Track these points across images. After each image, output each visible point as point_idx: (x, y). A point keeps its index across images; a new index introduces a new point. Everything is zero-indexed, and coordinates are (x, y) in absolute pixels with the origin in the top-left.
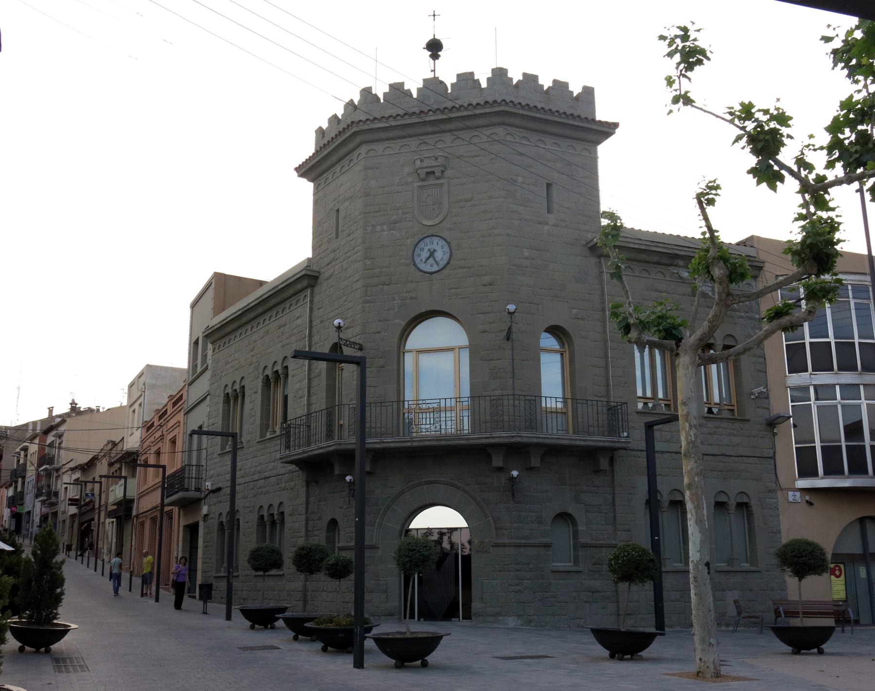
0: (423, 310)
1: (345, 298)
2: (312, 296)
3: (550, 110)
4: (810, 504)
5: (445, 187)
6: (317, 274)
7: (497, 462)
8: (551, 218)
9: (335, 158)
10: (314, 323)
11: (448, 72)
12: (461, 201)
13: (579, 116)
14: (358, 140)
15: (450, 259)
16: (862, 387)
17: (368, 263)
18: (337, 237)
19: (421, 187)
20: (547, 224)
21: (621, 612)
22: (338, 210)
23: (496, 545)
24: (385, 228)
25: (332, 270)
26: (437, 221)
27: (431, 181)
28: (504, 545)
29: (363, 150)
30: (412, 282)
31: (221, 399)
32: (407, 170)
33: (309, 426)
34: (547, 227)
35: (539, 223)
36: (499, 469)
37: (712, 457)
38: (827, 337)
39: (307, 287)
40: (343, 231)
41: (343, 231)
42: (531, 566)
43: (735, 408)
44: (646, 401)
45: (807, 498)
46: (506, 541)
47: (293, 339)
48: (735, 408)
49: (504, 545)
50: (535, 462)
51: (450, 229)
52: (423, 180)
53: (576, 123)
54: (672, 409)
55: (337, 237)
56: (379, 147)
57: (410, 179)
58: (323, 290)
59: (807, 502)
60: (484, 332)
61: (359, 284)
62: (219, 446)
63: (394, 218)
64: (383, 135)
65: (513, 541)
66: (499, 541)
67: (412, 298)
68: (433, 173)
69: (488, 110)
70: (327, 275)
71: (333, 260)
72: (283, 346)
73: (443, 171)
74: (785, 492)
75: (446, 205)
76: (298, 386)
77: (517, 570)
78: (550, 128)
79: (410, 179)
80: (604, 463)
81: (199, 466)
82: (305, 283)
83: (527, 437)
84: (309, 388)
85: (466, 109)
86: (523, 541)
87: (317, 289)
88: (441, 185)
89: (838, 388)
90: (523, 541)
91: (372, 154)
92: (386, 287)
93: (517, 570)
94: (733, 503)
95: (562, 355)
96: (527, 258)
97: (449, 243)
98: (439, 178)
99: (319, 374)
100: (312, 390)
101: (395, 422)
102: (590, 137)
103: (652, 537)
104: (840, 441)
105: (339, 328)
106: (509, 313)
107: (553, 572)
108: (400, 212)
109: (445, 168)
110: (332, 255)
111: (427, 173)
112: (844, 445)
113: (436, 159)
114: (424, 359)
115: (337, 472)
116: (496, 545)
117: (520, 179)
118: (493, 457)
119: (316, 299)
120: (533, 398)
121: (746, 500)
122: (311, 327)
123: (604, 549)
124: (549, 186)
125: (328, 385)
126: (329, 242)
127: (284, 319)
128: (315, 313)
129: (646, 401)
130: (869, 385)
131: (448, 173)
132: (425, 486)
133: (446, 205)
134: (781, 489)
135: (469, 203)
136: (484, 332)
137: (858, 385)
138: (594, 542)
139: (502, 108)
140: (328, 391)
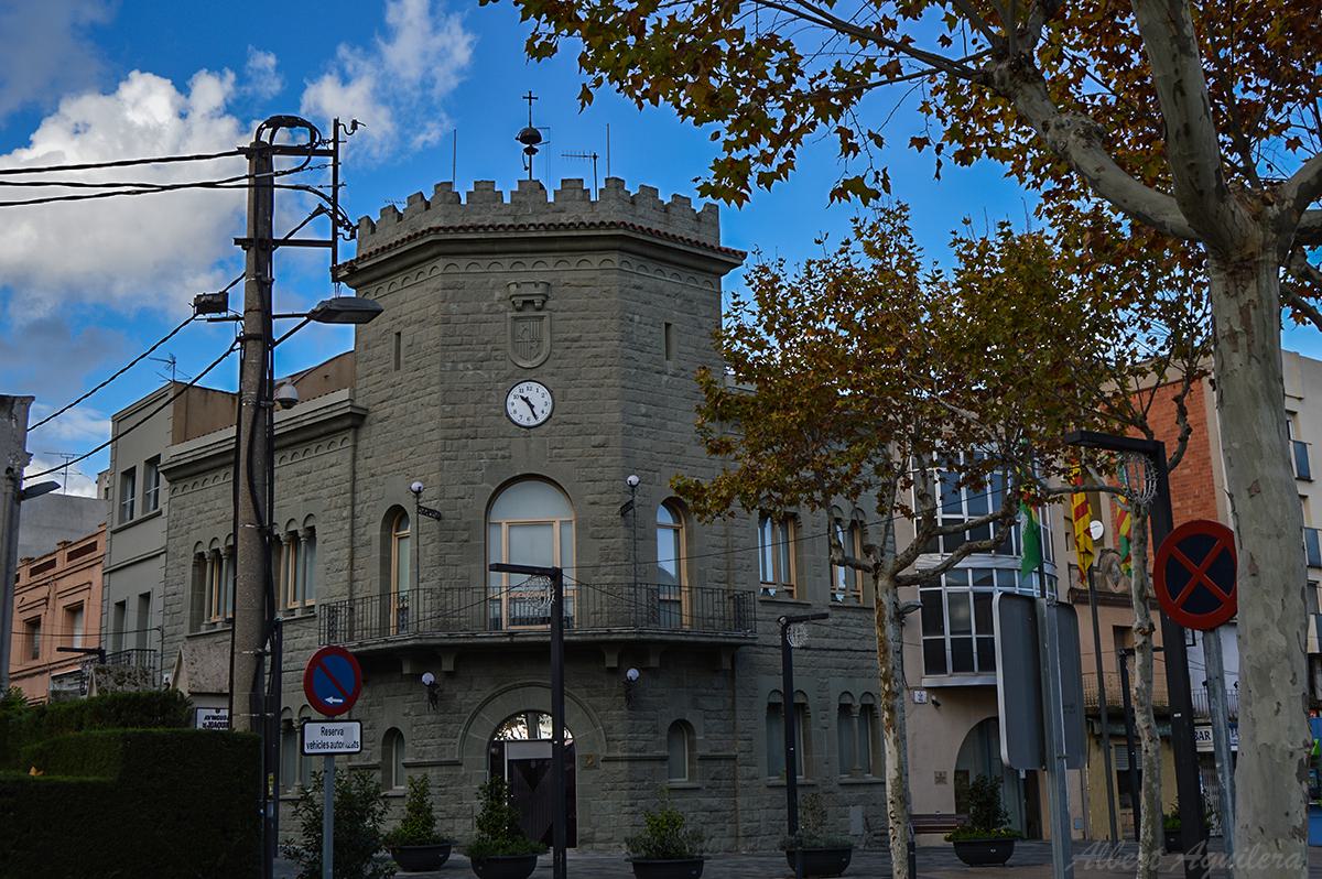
0: (518, 474)
1: (411, 449)
2: (356, 440)
3: (674, 236)
4: (936, 704)
5: (546, 320)
6: (364, 413)
7: (612, 662)
8: (671, 366)
9: (396, 266)
10: (359, 476)
11: (551, 172)
12: (566, 340)
13: (705, 244)
14: (434, 250)
15: (552, 413)
16: (994, 571)
17: (448, 409)
18: (398, 367)
19: (516, 319)
20: (666, 374)
21: (741, 834)
22: (399, 334)
23: (607, 760)
24: (469, 366)
25: (388, 410)
26: (536, 362)
27: (529, 312)
28: (616, 760)
29: (441, 263)
30: (503, 437)
31: (190, 561)
32: (497, 295)
33: (352, 609)
34: (665, 378)
35: (657, 373)
36: (612, 670)
37: (836, 653)
38: (961, 513)
39: (348, 428)
40: (407, 362)
41: (407, 362)
42: (646, 783)
43: (861, 594)
44: (766, 586)
45: (934, 698)
46: (619, 754)
47: (325, 492)
48: (861, 594)
49: (616, 760)
50: (654, 662)
51: (552, 375)
52: (519, 310)
53: (700, 252)
54: (795, 596)
55: (398, 367)
56: (462, 263)
57: (502, 307)
58: (371, 437)
59: (933, 702)
60: (592, 504)
61: (436, 435)
62: (187, 622)
63: (481, 354)
64: (469, 248)
65: (626, 754)
66: (611, 755)
67: (504, 457)
68: (532, 302)
69: (602, 233)
70: (380, 415)
71: (390, 398)
72: (306, 500)
73: (544, 302)
74: (911, 691)
75: (547, 342)
76: (333, 555)
77: (632, 789)
78: (671, 257)
79: (502, 307)
80: (726, 664)
81: (141, 650)
82: (348, 422)
83: (651, 633)
84: (352, 559)
85: (577, 228)
86: (638, 754)
87: (363, 432)
88: (542, 317)
89: (970, 572)
90: (638, 754)
91: (452, 269)
92: (470, 441)
93: (632, 789)
94: (857, 704)
95: (677, 531)
96: (643, 416)
97: (551, 392)
98: (539, 309)
99: (369, 543)
100: (356, 564)
101: (301, 560)
102: (715, 268)
103: (788, 750)
104: (970, 632)
105: (418, 493)
106: (631, 485)
107: (841, 785)
108: (489, 347)
109: (547, 297)
110: (390, 391)
111: (524, 302)
112: (974, 636)
113: (536, 285)
114: (517, 533)
115: (407, 670)
116: (607, 760)
117: (637, 318)
118: (607, 657)
119: (362, 444)
120: (656, 587)
121: (871, 702)
122: (354, 479)
123: (723, 762)
124: (668, 325)
125: (382, 558)
126: (385, 372)
127: (307, 464)
128: (361, 462)
129: (766, 586)
130: (1002, 569)
131: (550, 304)
132: (520, 690)
133: (547, 342)
134: (908, 688)
135: (577, 344)
136: (592, 504)
137: (991, 569)
138: (713, 754)
139: (621, 232)
140: (382, 564)
